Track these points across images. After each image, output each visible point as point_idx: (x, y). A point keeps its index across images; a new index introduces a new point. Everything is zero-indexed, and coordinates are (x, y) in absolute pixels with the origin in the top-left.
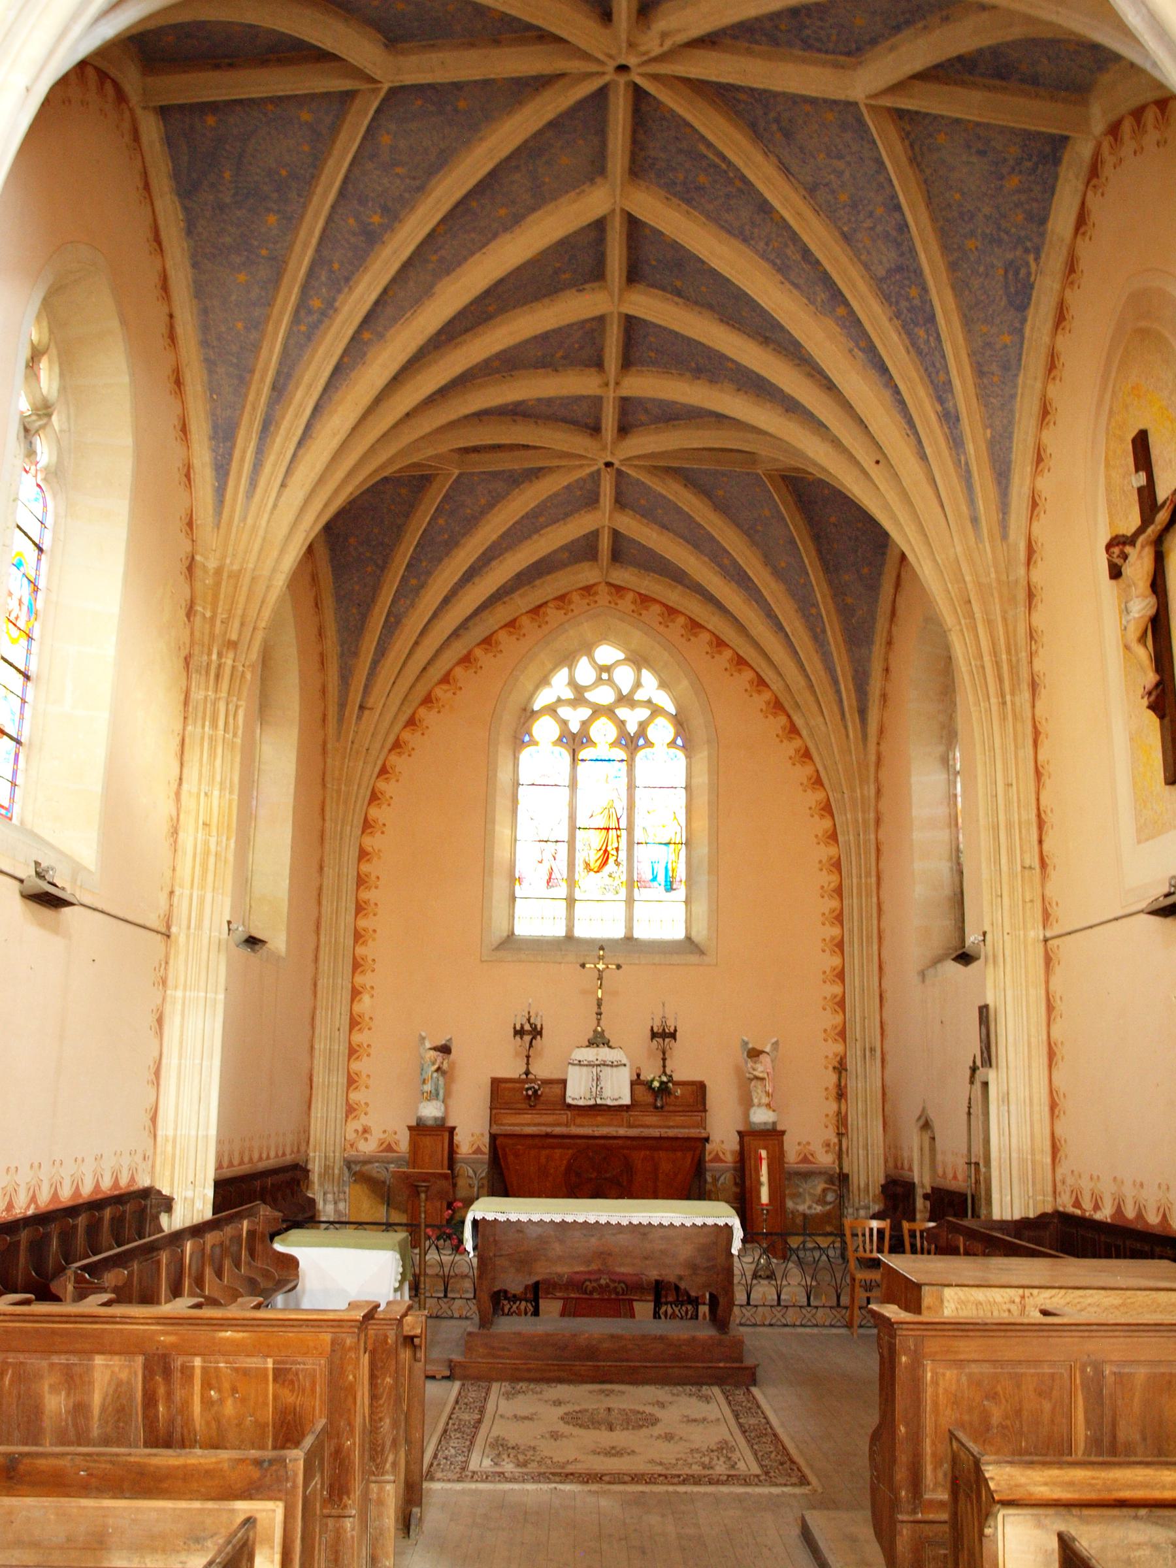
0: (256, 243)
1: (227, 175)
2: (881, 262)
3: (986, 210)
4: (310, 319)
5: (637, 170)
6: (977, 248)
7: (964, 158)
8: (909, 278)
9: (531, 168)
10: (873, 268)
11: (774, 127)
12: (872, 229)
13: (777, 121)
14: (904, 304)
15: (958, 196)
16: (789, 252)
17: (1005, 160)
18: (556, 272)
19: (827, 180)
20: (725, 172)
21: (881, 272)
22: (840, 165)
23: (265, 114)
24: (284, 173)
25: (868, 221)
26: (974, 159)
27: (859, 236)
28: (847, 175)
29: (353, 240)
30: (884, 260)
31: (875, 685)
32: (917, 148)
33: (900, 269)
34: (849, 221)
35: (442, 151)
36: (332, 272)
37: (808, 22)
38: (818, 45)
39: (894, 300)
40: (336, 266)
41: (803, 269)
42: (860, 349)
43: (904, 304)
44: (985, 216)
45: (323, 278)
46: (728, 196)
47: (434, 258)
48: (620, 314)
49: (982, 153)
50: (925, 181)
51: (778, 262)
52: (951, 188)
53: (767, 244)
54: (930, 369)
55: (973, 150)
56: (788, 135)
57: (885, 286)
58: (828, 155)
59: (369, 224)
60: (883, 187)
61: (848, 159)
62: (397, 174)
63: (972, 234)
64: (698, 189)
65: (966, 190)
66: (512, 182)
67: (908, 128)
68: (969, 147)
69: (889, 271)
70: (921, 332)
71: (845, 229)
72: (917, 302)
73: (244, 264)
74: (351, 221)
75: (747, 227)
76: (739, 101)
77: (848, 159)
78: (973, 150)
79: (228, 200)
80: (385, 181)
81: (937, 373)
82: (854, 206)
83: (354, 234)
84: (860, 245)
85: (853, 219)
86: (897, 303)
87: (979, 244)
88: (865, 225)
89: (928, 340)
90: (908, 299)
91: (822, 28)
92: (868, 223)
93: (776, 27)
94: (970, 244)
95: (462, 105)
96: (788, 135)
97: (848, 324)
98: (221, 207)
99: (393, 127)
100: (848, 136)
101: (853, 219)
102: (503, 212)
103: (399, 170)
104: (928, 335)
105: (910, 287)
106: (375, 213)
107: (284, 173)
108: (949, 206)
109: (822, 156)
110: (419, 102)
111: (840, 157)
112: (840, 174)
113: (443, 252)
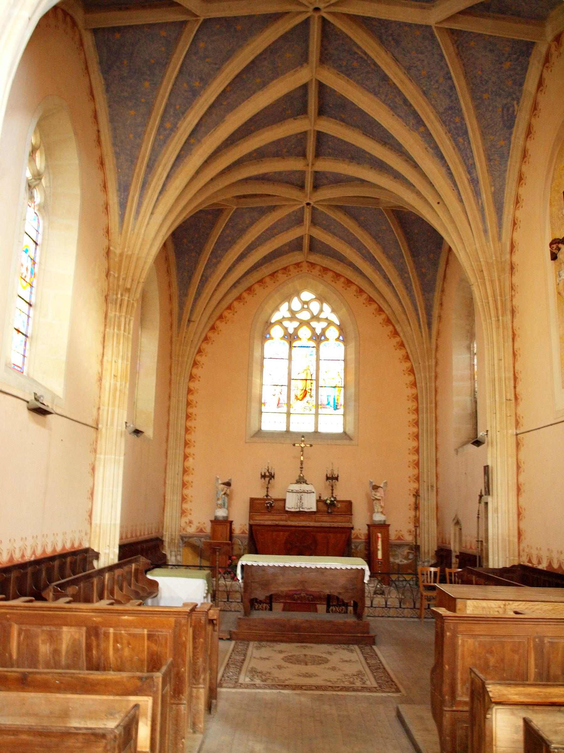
5: (324, 59)
12: (438, 88)
13: (392, 35)
14: (453, 126)
15: (479, 73)
16: (397, 100)
19: (416, 65)
21: (441, 110)
22: (420, 56)
23: (144, 33)
29: (186, 94)
30: (443, 104)
32: (460, 49)
33: (451, 108)
39: (447, 124)
40: (178, 107)
43: (453, 126)
46: (368, 73)
47: (225, 103)
49: (491, 51)
53: (386, 96)
56: (397, 42)
57: (443, 117)
63: (487, 91)
64: (353, 69)
67: (456, 38)
71: (424, 89)
72: (459, 125)
74: (185, 85)
81: (468, 159)
83: (186, 91)
86: (449, 125)
92: (436, 86)
96: (397, 42)
97: (425, 136)
99: (205, 38)
100: (426, 43)
102: (258, 80)
105: (455, 117)
110: (218, 26)
111: (422, 53)
113: (229, 100)
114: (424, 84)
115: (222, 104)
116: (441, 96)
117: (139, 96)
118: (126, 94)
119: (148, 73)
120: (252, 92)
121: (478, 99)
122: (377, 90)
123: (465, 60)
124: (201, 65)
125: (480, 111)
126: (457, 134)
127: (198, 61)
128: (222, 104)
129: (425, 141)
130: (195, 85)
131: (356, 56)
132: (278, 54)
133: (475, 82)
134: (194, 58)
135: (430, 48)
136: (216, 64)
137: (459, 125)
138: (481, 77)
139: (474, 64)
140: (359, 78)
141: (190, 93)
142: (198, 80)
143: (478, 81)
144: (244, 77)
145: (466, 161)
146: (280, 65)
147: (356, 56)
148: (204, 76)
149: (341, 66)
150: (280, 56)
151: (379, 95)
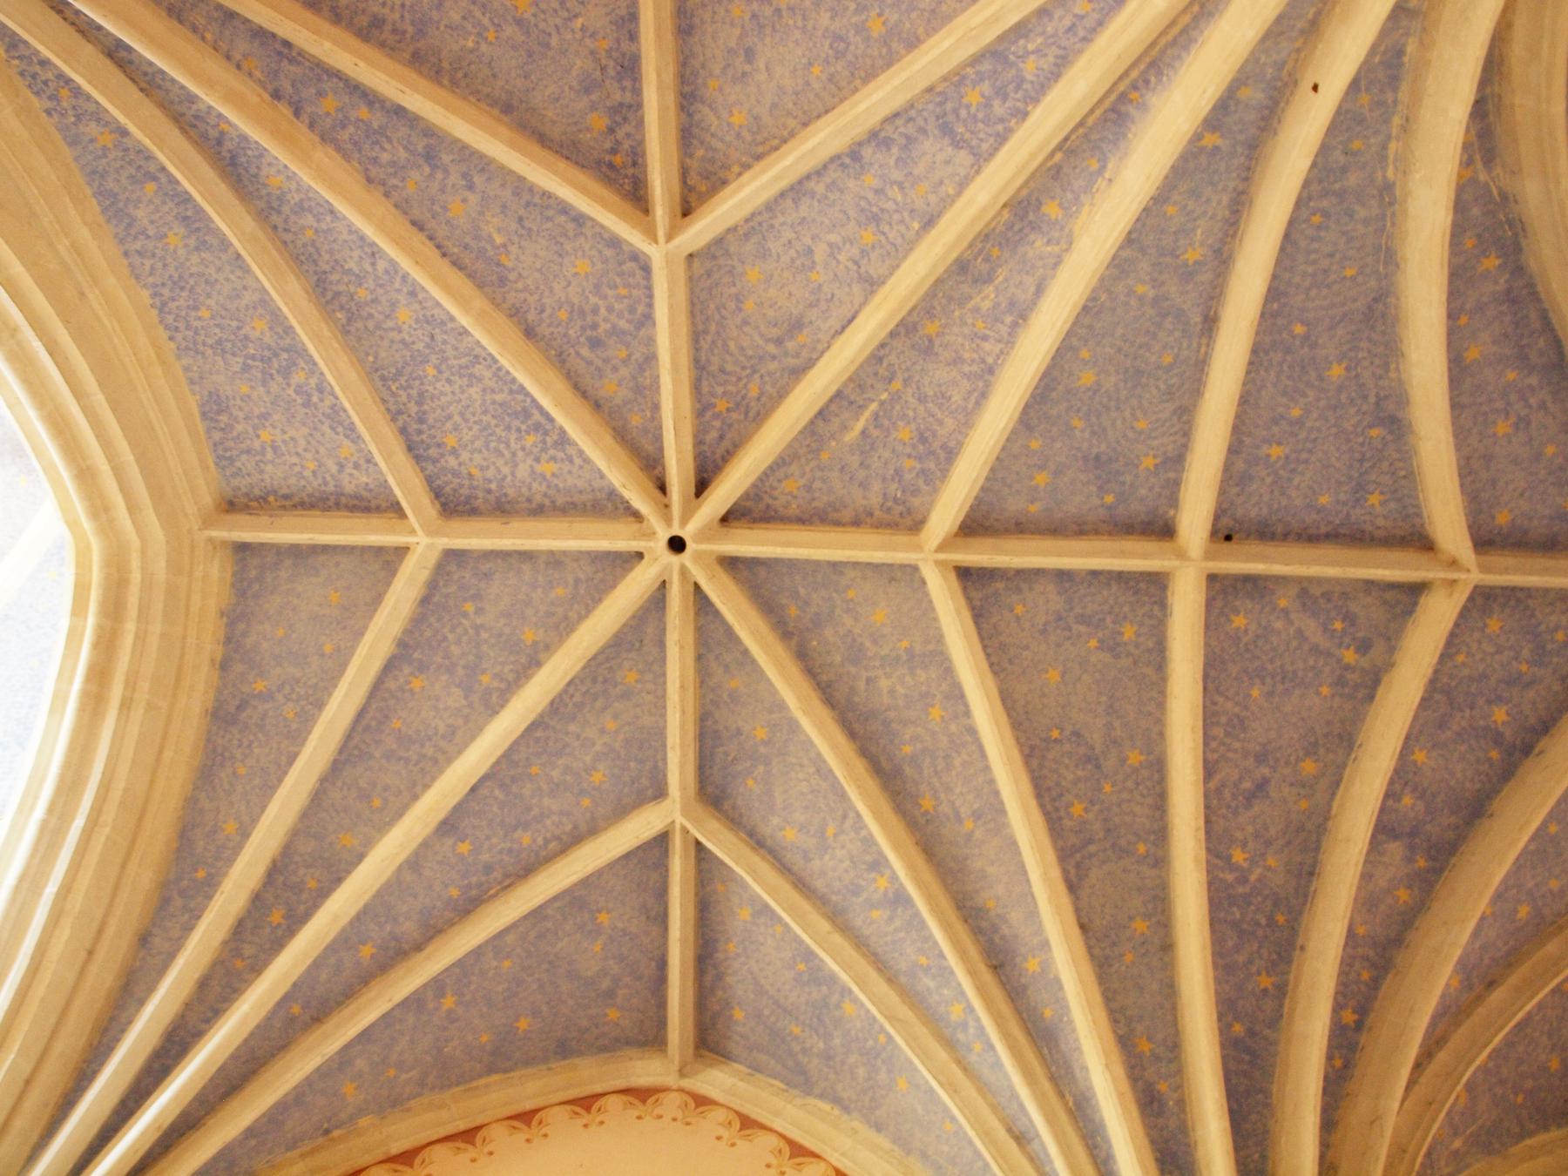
0: (871, 1043)
1: (797, 1030)
2: (948, 162)
3: (825, 19)
4: (971, 1030)
5: (913, 524)
6: (880, 15)
7: (762, 77)
8: (956, 111)
9: (877, 664)
10: (962, 172)
11: (790, 345)
12: (901, 186)
13: (779, 342)
14: (999, 109)
15: (816, 70)
16: (986, 304)
17: (754, 16)
18: (1112, 646)
19: (850, 265)
20: (882, 403)
21: (963, 157)
22: (820, 252)
23: (738, 955)
24: (802, 967)
25: (890, 193)
27: (919, 204)
29: (897, 923)
30: (940, 157)
31: (1253, 95)
32: (760, 149)
33: (946, 130)
34: (902, 221)
35: (818, 771)
36: (929, 968)
37: (604, 326)
38: (641, 309)
39: (1000, 128)
40: (923, 961)
41: (1006, 280)
43: (999, 109)
44: (832, 18)
45: (932, 984)
46: (922, 399)
47: (969, 825)
48: (1208, 556)
49: (750, 55)
50: (805, 125)
51: (1008, 319)
52: (807, 84)
53: (985, 338)
54: (1081, 33)
55: (748, 68)
56: (797, 325)
57: (985, 146)
58: (812, 268)
59: (885, 894)
60: (833, 182)
61: (808, 241)
62: (835, 835)
63: (861, 29)
64: (923, 439)
65: (804, 61)
66: (892, 691)
67: (736, 169)
68: (744, 74)
69: (958, 144)
70: (1030, 67)
71: (916, 225)
72: (986, 87)
73: (889, 1071)
74: (875, 914)
75: (966, 369)
76: (762, 394)
77: (808, 241)
78: (748, 68)
80: (839, 853)
81: (1082, 17)
83: (891, 919)
84: (933, 198)
85: (896, 217)
86: (1002, 120)
87: (873, 13)
88: (899, 198)
89: (1037, 51)
90: (988, 105)
91: (610, 309)
92: (894, 192)
93: (625, 362)
94: (877, 29)
95: (761, 734)
96: (797, 325)
97: (1069, 196)
98: (828, 1057)
99: (775, 821)
100: (774, 246)
101: (896, 217)
102: (936, 713)
103: (830, 831)
104: (1028, 53)
105: (968, 107)
106: (875, 880)
107: (802, 967)
108: (831, 79)
109: (813, 276)
110: (750, 782)
111: (810, 251)
113: (964, 811)
115: (969, 837)
116: (919, 170)
118: (861, 1072)
120: (969, 739)
121: (890, 48)
124: (839, 853)
125: (921, 30)
126: (1018, 88)
127: (827, 857)
128: (969, 837)
129: (1088, 189)
130: (882, 889)
131: (876, 433)
132: (868, 644)
133: (846, 73)
134: (816, 865)
135: (788, 234)
136: (845, 817)
137: (986, 87)
138: (827, 61)
139: (797, 94)
142: (873, 875)
143: (840, 66)
144: (908, 749)
145: (1089, 23)
146: (905, 644)
147: (876, 433)
148: (868, 858)
149: (923, 472)
150: (875, 642)
151: (990, 360)
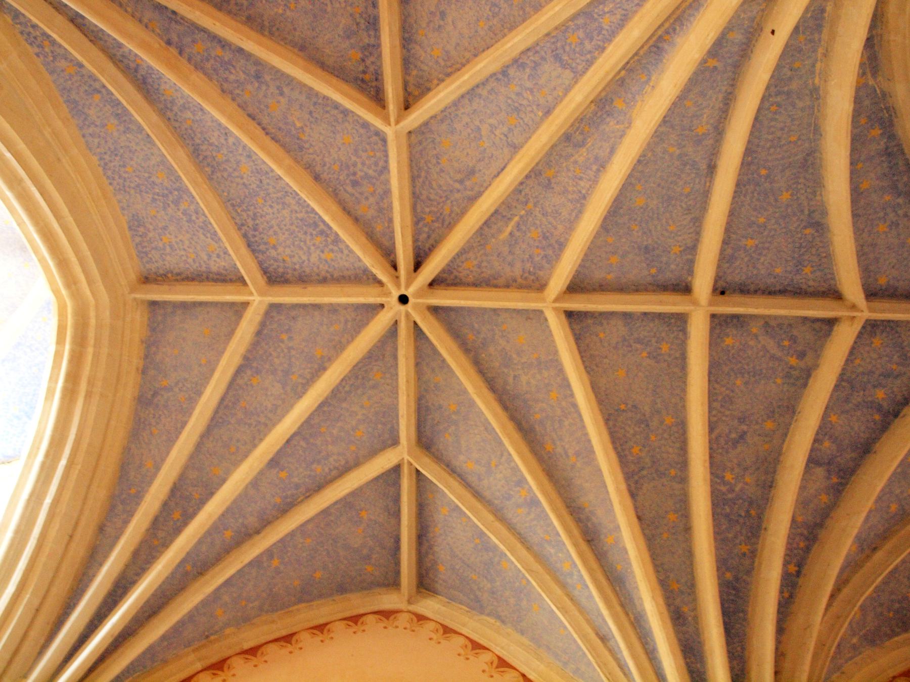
1: (474, 577)
2: (558, 77)
4: (575, 577)
5: (541, 286)
8: (563, 47)
10: (567, 82)
12: (531, 91)
14: (588, 46)
15: (481, 24)
16: (581, 160)
19: (502, 136)
20: (521, 217)
21: (568, 74)
26: (449, 19)
28: (492, 121)
29: (532, 516)
30: (554, 74)
32: (449, 70)
37: (360, 174)
39: (589, 56)
42: (650, 79)
43: (588, 46)
45: (552, 551)
46: (545, 214)
49: (443, 15)
50: (476, 56)
51: (595, 168)
53: (581, 179)
55: (442, 23)
56: (472, 172)
61: (477, 123)
64: (545, 238)
65: (475, 18)
66: (528, 383)
67: (435, 82)
68: (440, 26)
71: (540, 114)
72: (581, 33)
74: (520, 511)
75: (570, 197)
76: (452, 212)
77: (477, 123)
78: (442, 23)
79: (489, 585)
80: (498, 476)
82: (517, 110)
83: (529, 513)
85: (529, 109)
86: (590, 52)
88: (531, 98)
91: (363, 164)
92: (527, 95)
96: (472, 172)
97: (630, 96)
99: (462, 458)
100: (458, 126)
112: (493, 128)
113: (571, 452)
114: (532, 115)
116: (542, 81)
117: (517, 584)
119: (491, 554)
122: (575, 196)
123: (467, 55)
124: (498, 476)
132: (514, 356)
140: (560, 227)
141: (533, 509)
143: (495, 21)
147: (518, 234)
